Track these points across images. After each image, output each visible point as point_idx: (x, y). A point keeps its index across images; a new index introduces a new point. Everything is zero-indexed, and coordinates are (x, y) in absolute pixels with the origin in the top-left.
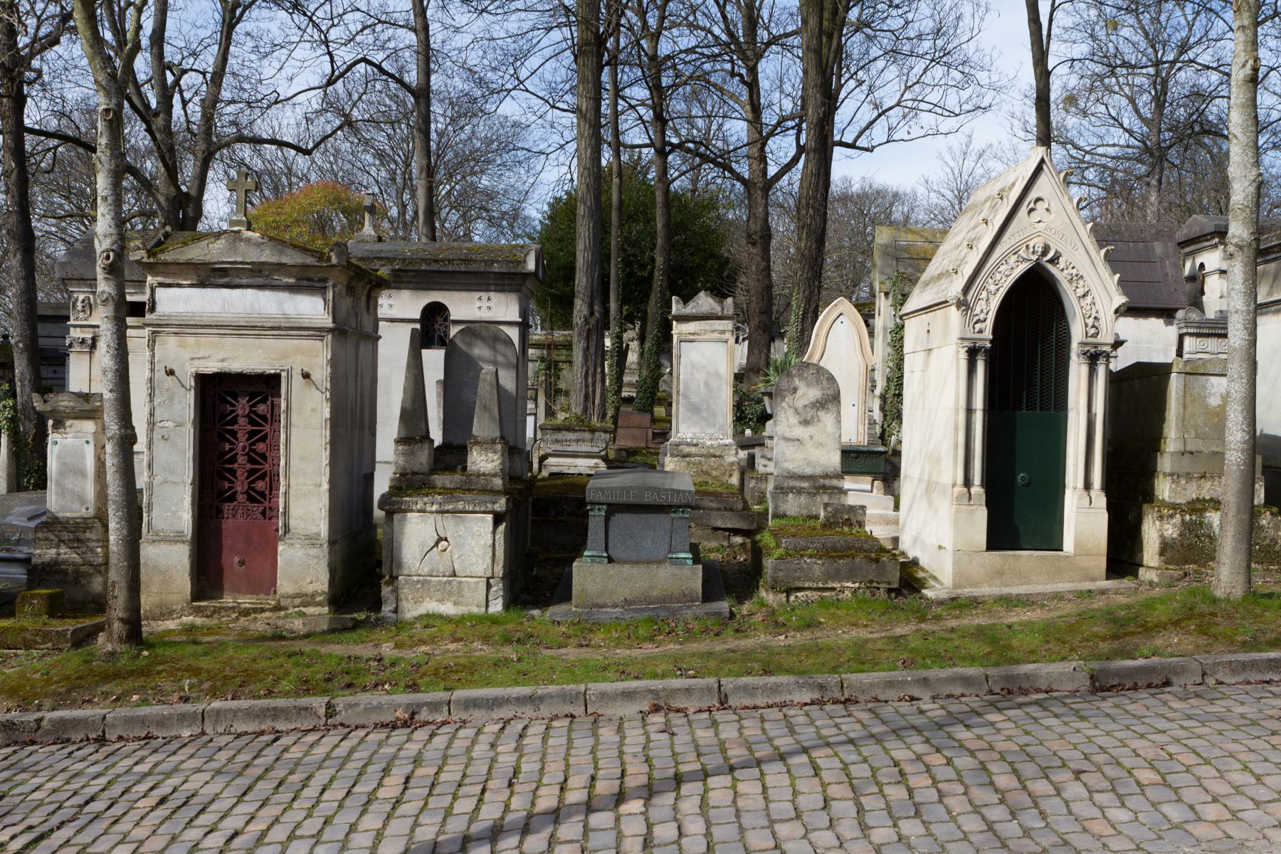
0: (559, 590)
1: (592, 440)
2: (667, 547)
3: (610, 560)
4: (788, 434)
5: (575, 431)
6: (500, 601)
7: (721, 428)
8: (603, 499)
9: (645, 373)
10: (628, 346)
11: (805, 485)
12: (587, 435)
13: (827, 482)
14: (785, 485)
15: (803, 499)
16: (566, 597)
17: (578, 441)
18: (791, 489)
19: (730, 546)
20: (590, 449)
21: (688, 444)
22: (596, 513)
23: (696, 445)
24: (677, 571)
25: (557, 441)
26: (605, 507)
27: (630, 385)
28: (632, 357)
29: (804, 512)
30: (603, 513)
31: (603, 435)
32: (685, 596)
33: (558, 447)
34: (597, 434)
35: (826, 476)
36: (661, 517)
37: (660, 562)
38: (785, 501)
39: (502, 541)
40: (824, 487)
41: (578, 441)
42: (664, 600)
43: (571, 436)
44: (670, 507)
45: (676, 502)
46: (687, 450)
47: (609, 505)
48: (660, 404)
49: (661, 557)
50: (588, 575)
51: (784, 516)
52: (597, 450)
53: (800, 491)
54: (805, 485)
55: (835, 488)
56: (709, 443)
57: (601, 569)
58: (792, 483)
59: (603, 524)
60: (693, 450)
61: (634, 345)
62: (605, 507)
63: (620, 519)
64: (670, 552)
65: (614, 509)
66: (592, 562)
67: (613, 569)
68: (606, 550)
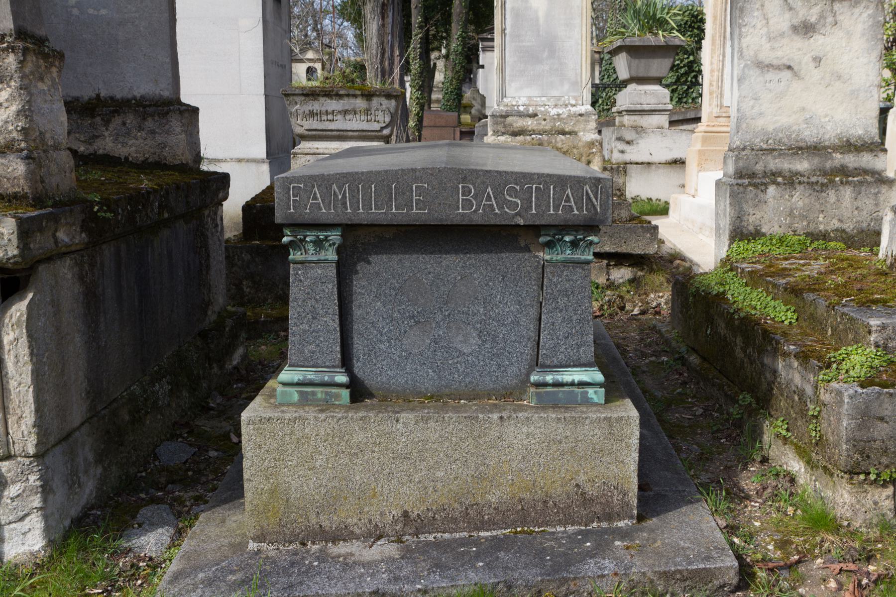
0: (207, 472)
1: (367, 111)
2: (528, 351)
3: (359, 392)
4: (766, 55)
5: (340, 96)
6: (36, 522)
7: (575, 84)
8: (326, 213)
9: (449, 73)
10: (435, 64)
11: (802, 165)
12: (360, 103)
13: (851, 160)
14: (759, 168)
15: (799, 198)
16: (234, 491)
17: (345, 112)
18: (773, 176)
19: (611, 285)
20: (365, 126)
21: (521, 115)
22: (311, 254)
23: (535, 115)
24: (562, 430)
25: (312, 114)
26: (335, 236)
27: (438, 101)
28: (439, 77)
29: (801, 226)
30: (331, 255)
31: (385, 102)
32: (586, 500)
33: (314, 124)
34: (375, 101)
35: (850, 146)
36: (508, 260)
37: (509, 395)
38: (759, 203)
39: (24, 350)
40: (843, 171)
41: (345, 112)
42: (527, 514)
43: (333, 105)
44: (535, 229)
45: (553, 213)
46: (519, 123)
47: (349, 229)
48: (466, 112)
49: (510, 381)
50: (288, 436)
51: (757, 235)
52: (376, 126)
53: (791, 180)
54: (802, 165)
55: (866, 172)
56: (553, 112)
57: (317, 426)
58: (773, 163)
59: (331, 287)
60: (529, 123)
61: (440, 64)
62: (335, 236)
63: (381, 271)
64: (536, 363)
65: (361, 241)
66: (305, 401)
67: (367, 427)
68: (346, 362)
